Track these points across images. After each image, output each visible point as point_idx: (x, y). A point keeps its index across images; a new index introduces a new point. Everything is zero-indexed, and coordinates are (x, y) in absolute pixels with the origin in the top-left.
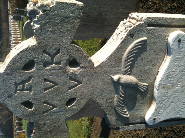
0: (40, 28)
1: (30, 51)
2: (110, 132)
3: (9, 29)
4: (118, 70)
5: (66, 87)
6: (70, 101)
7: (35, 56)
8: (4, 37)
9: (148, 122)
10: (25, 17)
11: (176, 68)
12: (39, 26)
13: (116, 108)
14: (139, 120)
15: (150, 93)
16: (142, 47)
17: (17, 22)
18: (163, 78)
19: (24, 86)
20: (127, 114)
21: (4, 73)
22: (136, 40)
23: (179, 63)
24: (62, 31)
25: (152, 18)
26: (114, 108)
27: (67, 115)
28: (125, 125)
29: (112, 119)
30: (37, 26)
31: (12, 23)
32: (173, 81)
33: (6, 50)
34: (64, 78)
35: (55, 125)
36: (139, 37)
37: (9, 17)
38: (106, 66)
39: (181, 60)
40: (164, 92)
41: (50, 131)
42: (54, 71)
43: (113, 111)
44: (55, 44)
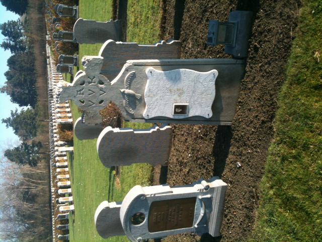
3: (47, 87)
6: (101, 102)
8: (39, 101)
10: (74, 67)
14: (140, 117)
16: (133, 76)
17: (61, 76)
20: (132, 112)
28: (133, 118)
29: (124, 114)
30: (86, 67)
31: (54, 77)
33: (43, 123)
36: (131, 71)
37: (49, 69)
44: (93, 74)
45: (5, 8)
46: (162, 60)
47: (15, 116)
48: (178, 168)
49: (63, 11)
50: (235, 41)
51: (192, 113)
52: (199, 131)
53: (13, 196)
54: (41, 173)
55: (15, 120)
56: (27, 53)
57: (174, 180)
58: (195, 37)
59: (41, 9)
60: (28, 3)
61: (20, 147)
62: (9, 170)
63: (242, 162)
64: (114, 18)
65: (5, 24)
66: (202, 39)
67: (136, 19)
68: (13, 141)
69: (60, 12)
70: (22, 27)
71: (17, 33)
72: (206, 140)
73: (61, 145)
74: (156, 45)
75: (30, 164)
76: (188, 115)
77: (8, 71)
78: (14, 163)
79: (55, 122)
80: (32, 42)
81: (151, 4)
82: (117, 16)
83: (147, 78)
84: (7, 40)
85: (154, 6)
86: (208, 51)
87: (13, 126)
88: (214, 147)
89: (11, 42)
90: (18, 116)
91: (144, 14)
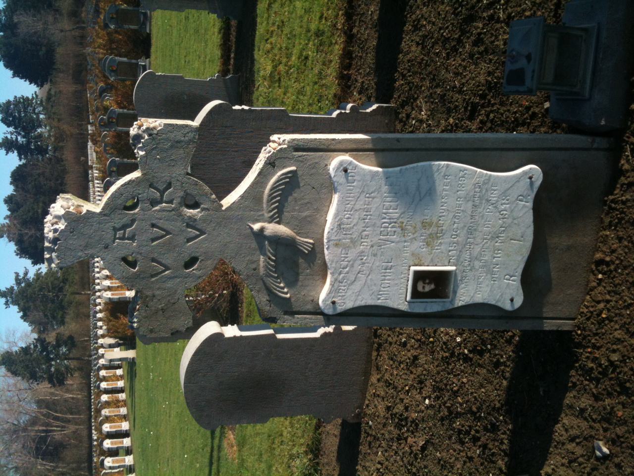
0: (145, 156)
1: (133, 185)
2: (357, 467)
4: (259, 216)
5: (181, 239)
7: (140, 192)
9: (323, 308)
11: (352, 212)
12: (144, 153)
13: (265, 279)
14: (309, 307)
15: (320, 257)
16: (291, 183)
18: (332, 229)
19: (124, 233)
21: (100, 212)
22: (280, 170)
23: (354, 205)
24: (173, 159)
25: (298, 140)
26: (262, 279)
27: (186, 284)
28: (286, 313)
30: (142, 153)
32: (351, 234)
33: (78, 297)
34: (179, 224)
35: (169, 300)
36: (284, 167)
37: (91, 191)
38: (240, 208)
39: (356, 201)
40: (339, 252)
41: (162, 309)
42: (164, 213)
43: (260, 285)
45: (10, 73)
46: (376, 136)
47: (23, 285)
48: (390, 432)
49: (117, 70)
50: (588, 81)
51: (466, 294)
52: (459, 339)
53: (15, 446)
54: (73, 398)
55: (22, 292)
56: (50, 159)
57: (379, 463)
58: (439, 91)
59: (80, 74)
60: (54, 63)
61: (32, 346)
62: (9, 394)
63: (612, 442)
64: (224, 72)
65: (9, 102)
66: (460, 92)
67: (275, 67)
68: (18, 335)
69: (113, 71)
70: (41, 109)
71: (32, 120)
72: (480, 366)
73: (111, 346)
74: (335, 114)
75: (51, 381)
76: (452, 302)
77: (12, 194)
78: (20, 378)
79: (99, 297)
80: (60, 137)
81: (313, 27)
82: (231, 67)
83: (331, 187)
84: (12, 133)
85: (321, 27)
86: (481, 122)
87: (18, 305)
88: (509, 388)
89: (19, 138)
90: (29, 284)
91: (296, 51)
